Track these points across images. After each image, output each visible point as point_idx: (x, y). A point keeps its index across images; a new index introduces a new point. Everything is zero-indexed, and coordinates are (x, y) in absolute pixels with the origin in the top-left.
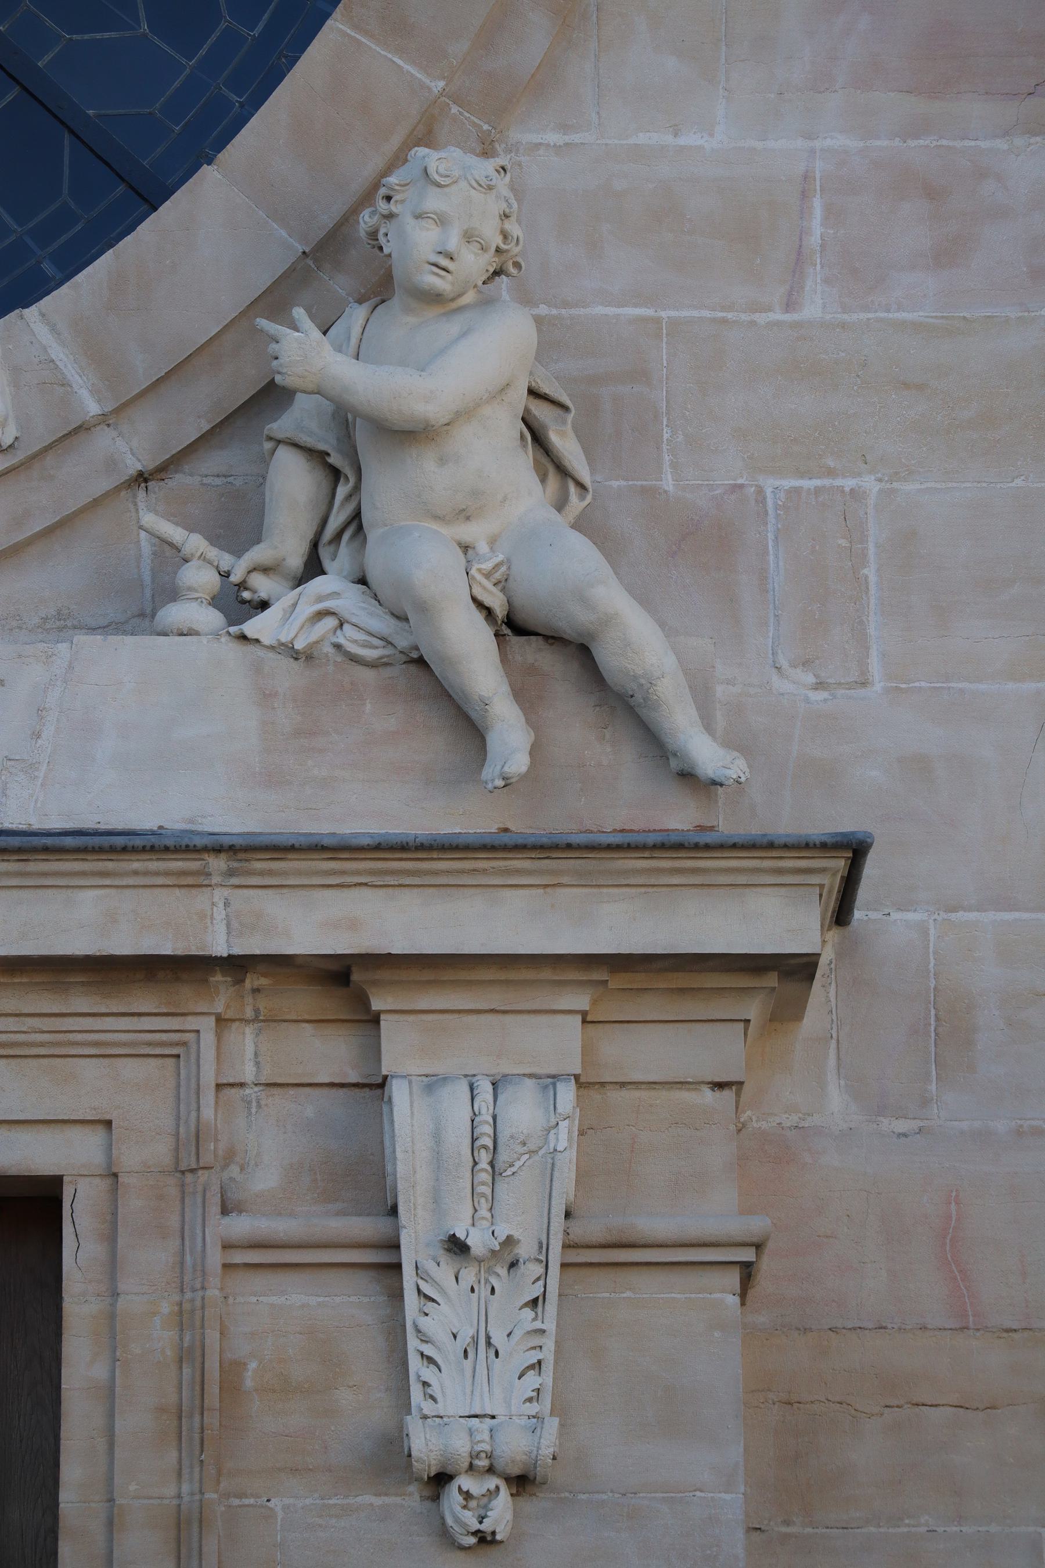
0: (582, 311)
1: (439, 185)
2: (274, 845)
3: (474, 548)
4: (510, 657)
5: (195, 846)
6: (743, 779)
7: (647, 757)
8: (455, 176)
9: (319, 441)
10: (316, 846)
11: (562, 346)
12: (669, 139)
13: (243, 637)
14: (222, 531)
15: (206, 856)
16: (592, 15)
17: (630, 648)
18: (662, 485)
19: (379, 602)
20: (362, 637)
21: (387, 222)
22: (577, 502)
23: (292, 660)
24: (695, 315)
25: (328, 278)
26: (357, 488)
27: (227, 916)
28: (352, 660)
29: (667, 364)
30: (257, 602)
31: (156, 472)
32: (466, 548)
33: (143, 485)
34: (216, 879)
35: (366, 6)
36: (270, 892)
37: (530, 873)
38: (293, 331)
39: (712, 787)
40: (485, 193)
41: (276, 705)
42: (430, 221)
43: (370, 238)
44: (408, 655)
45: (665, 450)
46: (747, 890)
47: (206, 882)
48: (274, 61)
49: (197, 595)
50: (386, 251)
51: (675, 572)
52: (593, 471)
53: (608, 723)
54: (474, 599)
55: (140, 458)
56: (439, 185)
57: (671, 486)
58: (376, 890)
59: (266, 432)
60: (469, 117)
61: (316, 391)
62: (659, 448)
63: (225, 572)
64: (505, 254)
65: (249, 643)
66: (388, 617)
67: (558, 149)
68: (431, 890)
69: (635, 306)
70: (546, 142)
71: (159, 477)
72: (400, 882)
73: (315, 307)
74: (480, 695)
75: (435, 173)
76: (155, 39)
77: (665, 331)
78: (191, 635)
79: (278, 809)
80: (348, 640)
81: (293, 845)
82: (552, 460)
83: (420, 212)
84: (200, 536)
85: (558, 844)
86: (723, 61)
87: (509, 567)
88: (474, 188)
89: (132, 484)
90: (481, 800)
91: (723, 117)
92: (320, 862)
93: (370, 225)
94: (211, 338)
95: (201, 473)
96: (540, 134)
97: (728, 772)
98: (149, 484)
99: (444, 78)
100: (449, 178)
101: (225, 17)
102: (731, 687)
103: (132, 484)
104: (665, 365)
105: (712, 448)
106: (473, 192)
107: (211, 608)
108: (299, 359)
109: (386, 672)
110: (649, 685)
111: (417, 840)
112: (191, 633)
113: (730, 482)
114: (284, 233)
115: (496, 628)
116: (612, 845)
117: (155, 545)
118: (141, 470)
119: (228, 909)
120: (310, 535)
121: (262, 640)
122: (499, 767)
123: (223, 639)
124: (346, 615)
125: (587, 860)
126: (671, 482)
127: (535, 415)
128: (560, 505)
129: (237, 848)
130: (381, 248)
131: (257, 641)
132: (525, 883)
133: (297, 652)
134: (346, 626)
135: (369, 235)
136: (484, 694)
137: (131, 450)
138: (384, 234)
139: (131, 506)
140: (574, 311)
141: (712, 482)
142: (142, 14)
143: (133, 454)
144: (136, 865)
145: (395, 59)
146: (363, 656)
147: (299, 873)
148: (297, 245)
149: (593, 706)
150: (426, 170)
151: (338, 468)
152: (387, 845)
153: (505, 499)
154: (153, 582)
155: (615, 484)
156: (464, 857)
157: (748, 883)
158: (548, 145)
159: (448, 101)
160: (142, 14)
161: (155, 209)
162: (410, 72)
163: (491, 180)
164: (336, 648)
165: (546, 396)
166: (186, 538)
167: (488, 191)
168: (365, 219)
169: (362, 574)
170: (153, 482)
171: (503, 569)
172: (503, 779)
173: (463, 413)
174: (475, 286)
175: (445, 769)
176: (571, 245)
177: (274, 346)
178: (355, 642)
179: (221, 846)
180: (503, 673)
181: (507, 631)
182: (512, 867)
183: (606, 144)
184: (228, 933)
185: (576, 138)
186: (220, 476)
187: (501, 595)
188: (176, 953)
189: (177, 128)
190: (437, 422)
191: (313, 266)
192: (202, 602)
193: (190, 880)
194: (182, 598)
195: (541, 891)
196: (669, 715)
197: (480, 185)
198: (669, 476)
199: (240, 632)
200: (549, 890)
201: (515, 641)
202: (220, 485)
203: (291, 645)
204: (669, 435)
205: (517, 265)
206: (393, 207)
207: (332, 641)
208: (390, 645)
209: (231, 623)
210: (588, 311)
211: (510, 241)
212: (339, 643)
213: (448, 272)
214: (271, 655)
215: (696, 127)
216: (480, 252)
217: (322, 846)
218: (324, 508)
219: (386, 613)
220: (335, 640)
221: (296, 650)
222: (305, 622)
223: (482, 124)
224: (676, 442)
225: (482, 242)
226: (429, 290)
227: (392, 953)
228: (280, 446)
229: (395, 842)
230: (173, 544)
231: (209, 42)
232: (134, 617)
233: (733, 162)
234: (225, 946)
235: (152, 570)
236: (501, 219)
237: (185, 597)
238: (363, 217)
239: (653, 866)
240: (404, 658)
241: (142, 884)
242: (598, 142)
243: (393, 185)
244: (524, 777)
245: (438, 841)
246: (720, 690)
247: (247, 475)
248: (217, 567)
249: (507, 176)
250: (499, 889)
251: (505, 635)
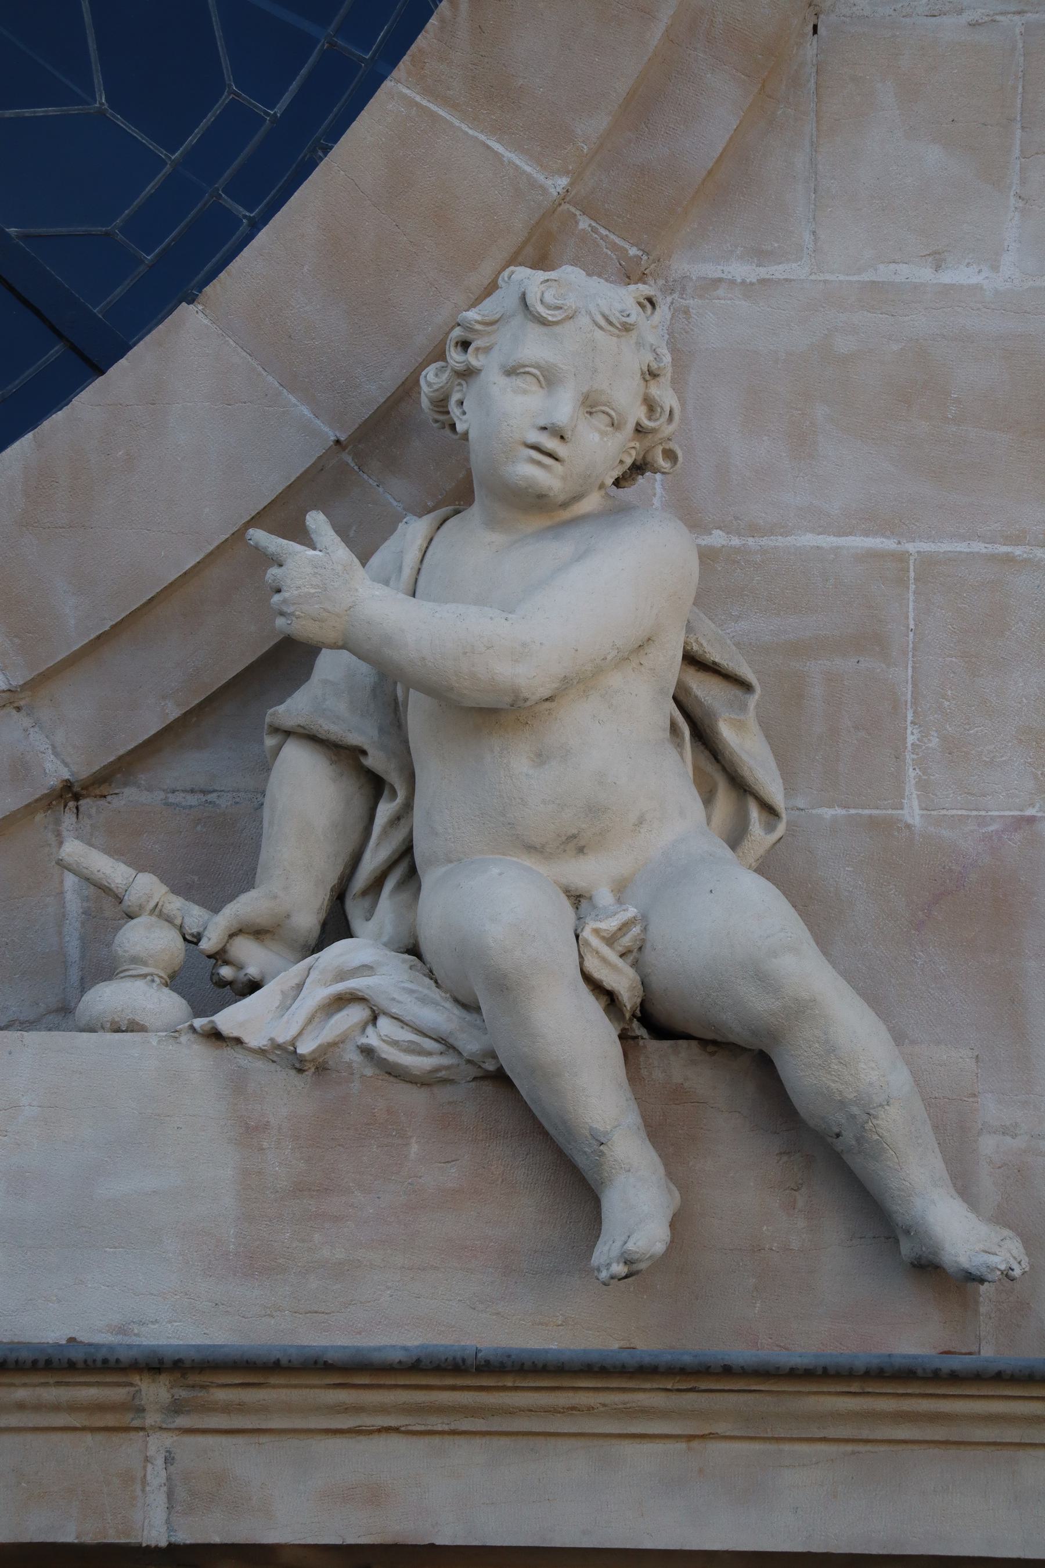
0: (780, 541)
1: (543, 322)
2: (247, 1362)
3: (591, 898)
4: (644, 1072)
5: (118, 1361)
6: (1017, 1272)
7: (864, 1237)
8: (571, 307)
9: (349, 730)
10: (316, 1362)
11: (747, 595)
12: (925, 274)
13: (215, 1036)
14: (196, 878)
15: (136, 1379)
16: (809, 81)
17: (835, 1055)
18: (903, 815)
19: (436, 982)
20: (406, 1036)
21: (463, 382)
22: (762, 833)
23: (293, 1073)
24: (962, 550)
25: (375, 484)
26: (408, 806)
27: (169, 1479)
28: (390, 1074)
29: (916, 625)
30: (242, 983)
31: (93, 784)
32: (577, 898)
33: (71, 804)
34: (151, 1419)
35: (446, 59)
36: (240, 1440)
37: (664, 1414)
38: (306, 548)
39: (971, 1285)
40: (618, 336)
41: (265, 1145)
42: (529, 378)
43: (436, 409)
44: (480, 1067)
45: (909, 761)
46: (1021, 1453)
47: (136, 1423)
48: (305, 156)
49: (145, 970)
50: (460, 427)
51: (921, 954)
52: (790, 790)
53: (800, 1181)
54: (588, 978)
55: (68, 760)
56: (543, 322)
57: (917, 818)
58: (414, 1439)
59: (268, 719)
60: (606, 235)
61: (340, 643)
62: (899, 757)
63: (192, 935)
64: (650, 436)
65: (225, 1044)
66: (449, 1005)
67: (748, 289)
68: (504, 1441)
69: (866, 533)
70: (730, 277)
71: (97, 792)
72: (453, 1427)
73: (354, 528)
74: (591, 1129)
75: (539, 302)
76: (118, 119)
77: (912, 574)
78: (132, 1031)
79: (264, 1312)
80: (384, 1041)
81: (278, 1360)
82: (724, 769)
83: (514, 364)
84: (155, 879)
85: (710, 1367)
86: (1016, 152)
87: (645, 929)
88: (601, 328)
89: (54, 803)
90: (593, 1301)
91: (1015, 241)
92: (323, 1391)
93: (436, 387)
94: (185, 573)
95: (166, 787)
96: (719, 265)
97: (993, 1260)
98: (81, 802)
99: (568, 174)
100: (560, 311)
101: (230, 86)
102: (1008, 1139)
103: (54, 803)
104: (912, 626)
105: (985, 759)
106: (599, 334)
107: (166, 991)
108: (312, 591)
109: (443, 1094)
110: (865, 1117)
111: (480, 1355)
112: (134, 1027)
113: (1012, 813)
114: (306, 411)
115: (622, 1025)
116: (798, 1369)
117: (87, 899)
118: (68, 781)
119: (171, 1468)
120: (332, 878)
121: (246, 1039)
122: (618, 1244)
123: (184, 1039)
124: (383, 1002)
125: (757, 1396)
126: (917, 811)
127: (696, 697)
128: (736, 838)
129: (187, 1366)
130: (453, 427)
131: (238, 1041)
132: (656, 1432)
133: (302, 1059)
134: (383, 1022)
135: (437, 406)
136: (599, 1126)
137: (54, 747)
138: (457, 401)
139: (51, 837)
140: (766, 542)
141: (983, 813)
142: (98, 79)
143: (56, 754)
144: (21, 1394)
145: (493, 144)
146: (407, 1067)
147: (288, 1409)
148: (326, 429)
149: (777, 1154)
150: (523, 298)
151: (380, 774)
152: (431, 1362)
153: (641, 821)
154: (83, 957)
155: (828, 813)
156: (556, 1385)
157: (1023, 1441)
158: (732, 282)
159: (573, 210)
160: (98, 79)
161: (102, 372)
162: (514, 164)
163: (628, 316)
164: (364, 1054)
165: (717, 668)
166: (131, 880)
167: (624, 333)
168: (428, 379)
169: (412, 941)
170: (88, 800)
171: (636, 930)
172: (625, 1263)
173: (575, 682)
174: (602, 486)
175: (536, 1252)
176: (765, 438)
177: (274, 571)
178: (395, 1043)
179: (161, 1361)
180: (629, 1094)
181: (641, 1031)
182: (634, 1405)
183: (825, 282)
184: (170, 1508)
185: (777, 271)
186: (196, 792)
187: (631, 972)
188: (82, 1541)
189: (149, 258)
190: (533, 694)
191: (352, 465)
192: (153, 981)
193: (110, 1420)
194: (122, 975)
195: (682, 1446)
196: (897, 1167)
197: (611, 323)
198: (915, 803)
199: (210, 1026)
200: (695, 1444)
201: (653, 1046)
202: (195, 806)
203: (292, 1048)
204: (915, 737)
205: (670, 455)
206: (472, 358)
207: (359, 1043)
208: (451, 1051)
209: (198, 1013)
210: (790, 540)
211: (658, 415)
212: (369, 1045)
213: (557, 459)
214: (260, 1064)
215: (970, 257)
216: (609, 429)
217: (325, 1363)
218: (355, 837)
219: (446, 999)
220: (363, 1040)
221: (301, 1055)
222: (316, 1012)
223: (627, 246)
224: (928, 748)
225: (613, 413)
226: (526, 488)
227: (437, 1543)
228: (289, 741)
229: (443, 1358)
230: (110, 890)
231: (205, 123)
232: (50, 1012)
233: (1028, 310)
234: (164, 1529)
235: (82, 939)
236: (644, 378)
237: (127, 973)
238: (426, 377)
239: (865, 1407)
240: (473, 1072)
241: (30, 1425)
242: (813, 277)
243: (473, 322)
244: (661, 1263)
245: (513, 1357)
246: (988, 1145)
247: (238, 791)
248: (181, 928)
249: (656, 313)
250: (614, 1441)
251: (636, 1037)
